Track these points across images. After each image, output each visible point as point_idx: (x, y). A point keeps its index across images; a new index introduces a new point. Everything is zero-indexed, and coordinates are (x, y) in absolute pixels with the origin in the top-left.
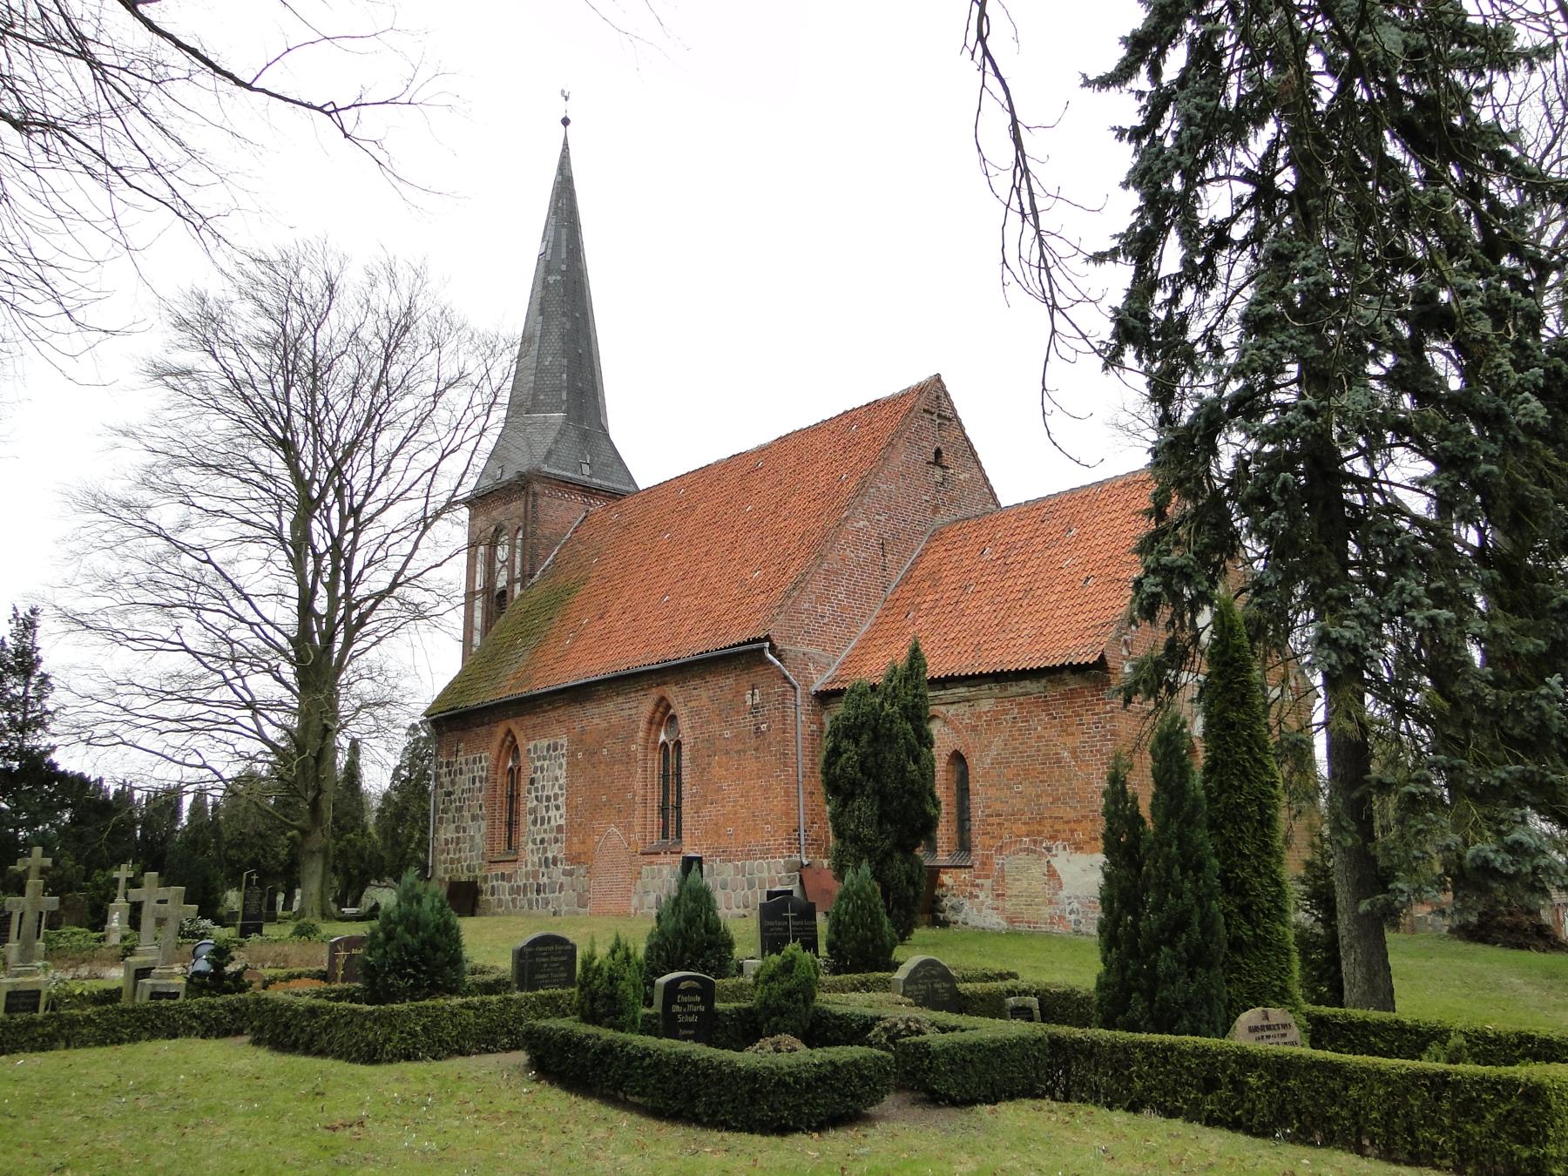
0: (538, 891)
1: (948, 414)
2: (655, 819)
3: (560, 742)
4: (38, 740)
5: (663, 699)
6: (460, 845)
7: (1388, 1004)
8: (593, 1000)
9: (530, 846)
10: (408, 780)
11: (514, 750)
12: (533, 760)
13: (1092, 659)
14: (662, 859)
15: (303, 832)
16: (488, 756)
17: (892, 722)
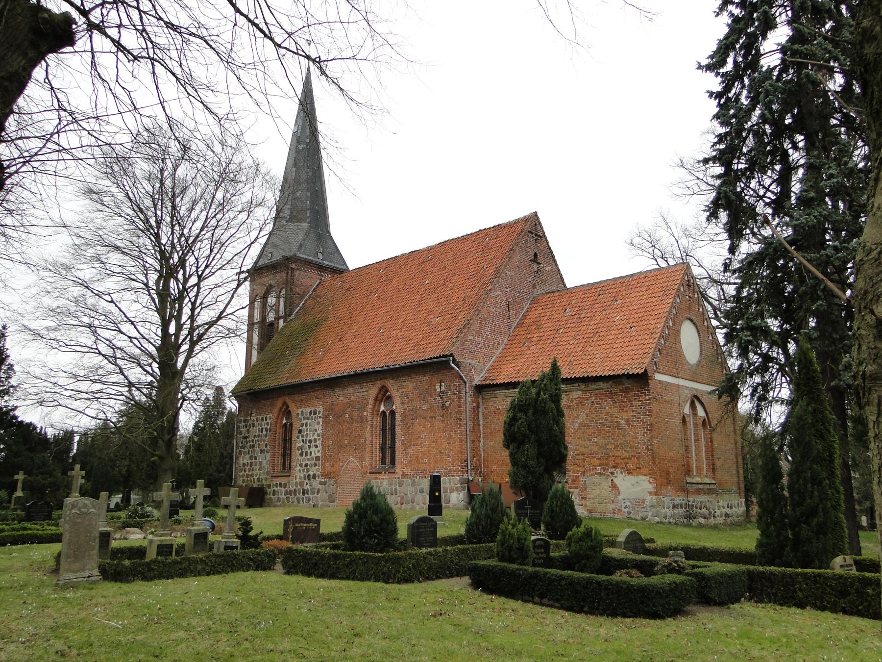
0: (304, 493)
1: (540, 234)
2: (378, 454)
5: (383, 387)
6: (254, 464)
7: (861, 555)
8: (510, 551)
9: (299, 468)
11: (288, 413)
12: (300, 419)
13: (641, 371)
17: (545, 403)
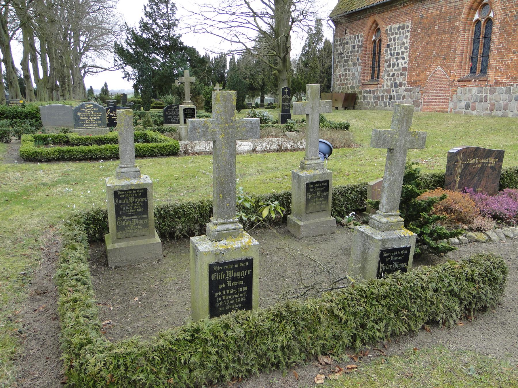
0: (390, 99)
2: (467, 63)
3: (406, 24)
4: (175, 32)
9: (386, 77)
10: (308, 51)
12: (389, 35)
14: (472, 83)
15: (279, 71)
16: (362, 35)
